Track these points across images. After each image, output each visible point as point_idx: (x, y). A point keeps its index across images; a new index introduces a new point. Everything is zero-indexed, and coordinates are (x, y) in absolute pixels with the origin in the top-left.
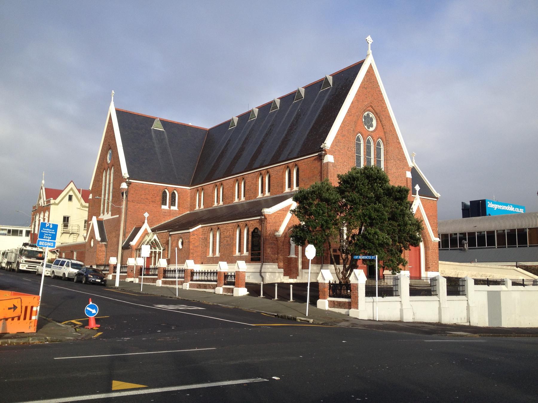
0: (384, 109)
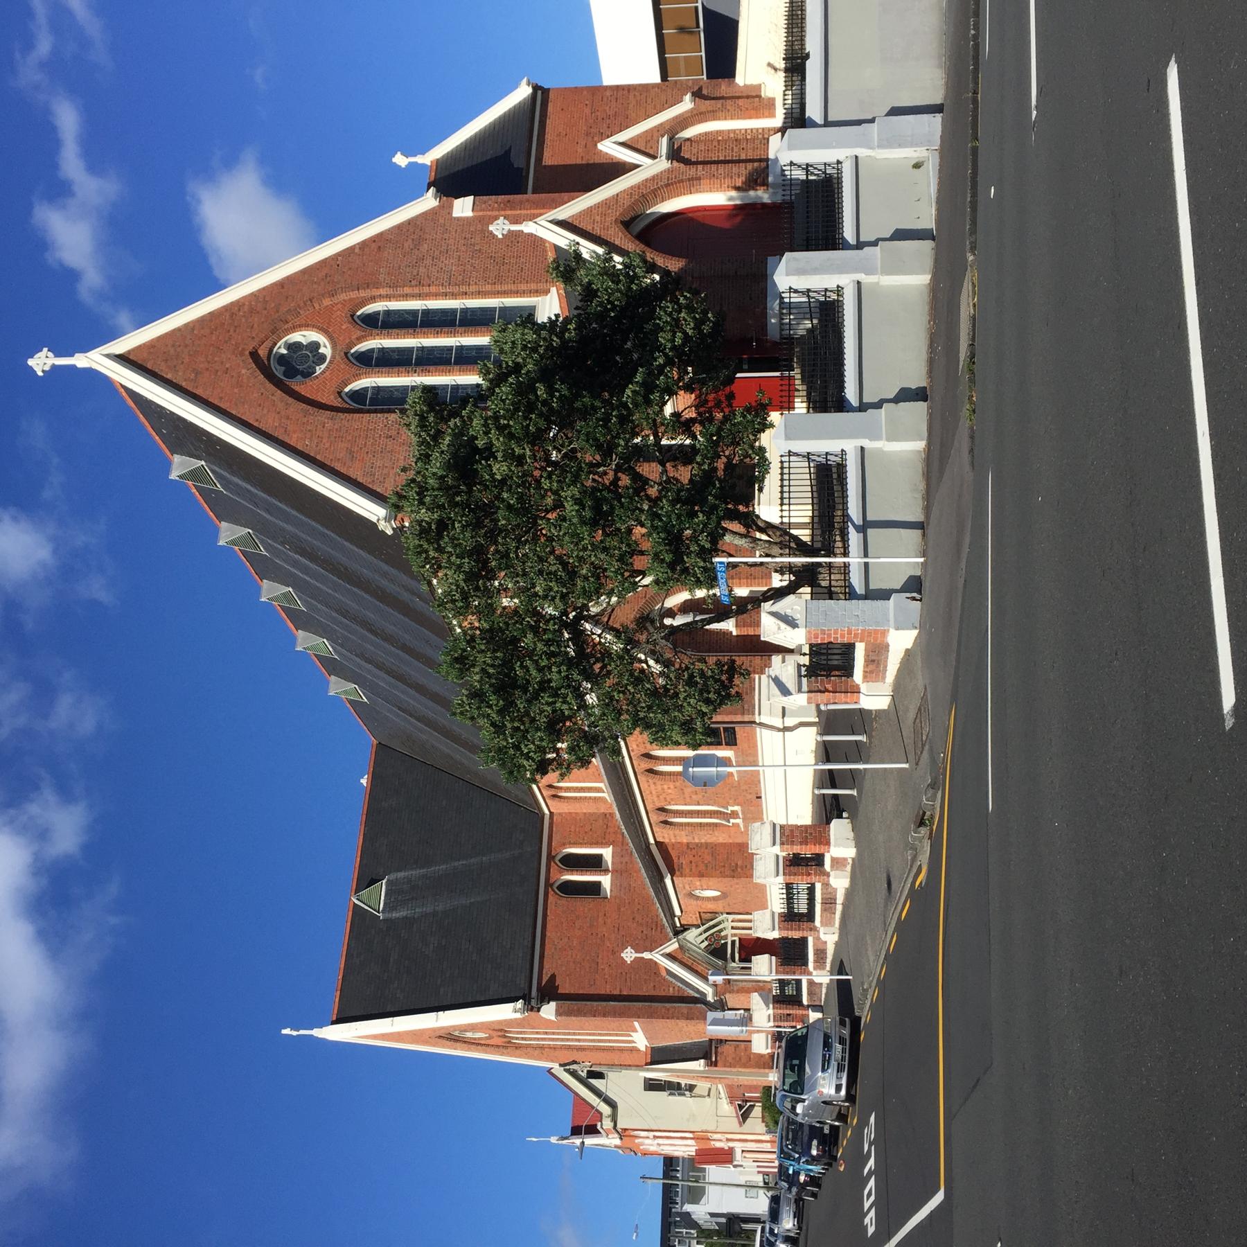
0: (259, 304)
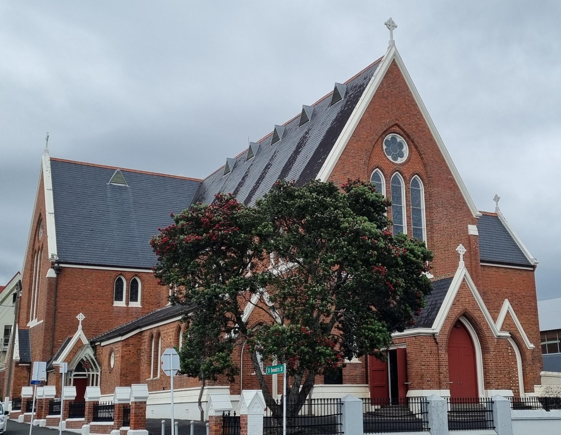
0: (421, 128)
